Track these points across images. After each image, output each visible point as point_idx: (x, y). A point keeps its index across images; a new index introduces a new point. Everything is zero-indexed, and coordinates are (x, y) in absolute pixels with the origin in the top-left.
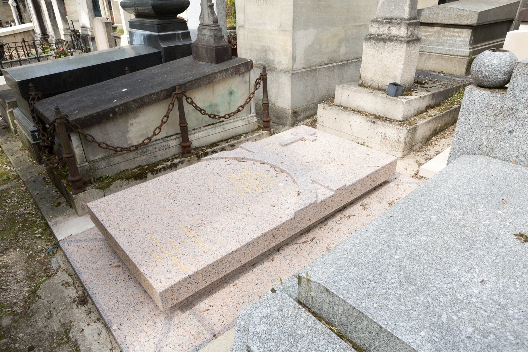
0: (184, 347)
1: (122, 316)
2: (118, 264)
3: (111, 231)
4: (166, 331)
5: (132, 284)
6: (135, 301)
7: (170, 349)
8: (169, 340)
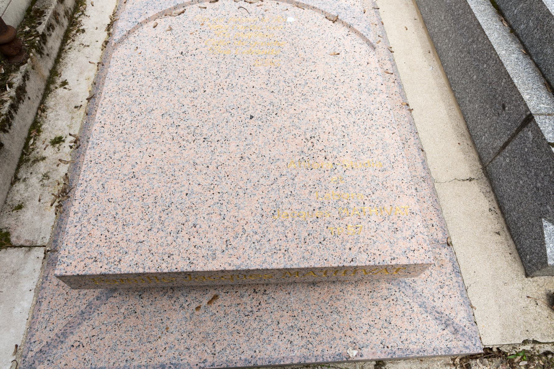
0: (447, 283)
1: (337, 335)
2: (209, 296)
3: (95, 269)
4: (411, 291)
5: (384, 287)
6: (323, 305)
7: (440, 300)
8: (426, 293)
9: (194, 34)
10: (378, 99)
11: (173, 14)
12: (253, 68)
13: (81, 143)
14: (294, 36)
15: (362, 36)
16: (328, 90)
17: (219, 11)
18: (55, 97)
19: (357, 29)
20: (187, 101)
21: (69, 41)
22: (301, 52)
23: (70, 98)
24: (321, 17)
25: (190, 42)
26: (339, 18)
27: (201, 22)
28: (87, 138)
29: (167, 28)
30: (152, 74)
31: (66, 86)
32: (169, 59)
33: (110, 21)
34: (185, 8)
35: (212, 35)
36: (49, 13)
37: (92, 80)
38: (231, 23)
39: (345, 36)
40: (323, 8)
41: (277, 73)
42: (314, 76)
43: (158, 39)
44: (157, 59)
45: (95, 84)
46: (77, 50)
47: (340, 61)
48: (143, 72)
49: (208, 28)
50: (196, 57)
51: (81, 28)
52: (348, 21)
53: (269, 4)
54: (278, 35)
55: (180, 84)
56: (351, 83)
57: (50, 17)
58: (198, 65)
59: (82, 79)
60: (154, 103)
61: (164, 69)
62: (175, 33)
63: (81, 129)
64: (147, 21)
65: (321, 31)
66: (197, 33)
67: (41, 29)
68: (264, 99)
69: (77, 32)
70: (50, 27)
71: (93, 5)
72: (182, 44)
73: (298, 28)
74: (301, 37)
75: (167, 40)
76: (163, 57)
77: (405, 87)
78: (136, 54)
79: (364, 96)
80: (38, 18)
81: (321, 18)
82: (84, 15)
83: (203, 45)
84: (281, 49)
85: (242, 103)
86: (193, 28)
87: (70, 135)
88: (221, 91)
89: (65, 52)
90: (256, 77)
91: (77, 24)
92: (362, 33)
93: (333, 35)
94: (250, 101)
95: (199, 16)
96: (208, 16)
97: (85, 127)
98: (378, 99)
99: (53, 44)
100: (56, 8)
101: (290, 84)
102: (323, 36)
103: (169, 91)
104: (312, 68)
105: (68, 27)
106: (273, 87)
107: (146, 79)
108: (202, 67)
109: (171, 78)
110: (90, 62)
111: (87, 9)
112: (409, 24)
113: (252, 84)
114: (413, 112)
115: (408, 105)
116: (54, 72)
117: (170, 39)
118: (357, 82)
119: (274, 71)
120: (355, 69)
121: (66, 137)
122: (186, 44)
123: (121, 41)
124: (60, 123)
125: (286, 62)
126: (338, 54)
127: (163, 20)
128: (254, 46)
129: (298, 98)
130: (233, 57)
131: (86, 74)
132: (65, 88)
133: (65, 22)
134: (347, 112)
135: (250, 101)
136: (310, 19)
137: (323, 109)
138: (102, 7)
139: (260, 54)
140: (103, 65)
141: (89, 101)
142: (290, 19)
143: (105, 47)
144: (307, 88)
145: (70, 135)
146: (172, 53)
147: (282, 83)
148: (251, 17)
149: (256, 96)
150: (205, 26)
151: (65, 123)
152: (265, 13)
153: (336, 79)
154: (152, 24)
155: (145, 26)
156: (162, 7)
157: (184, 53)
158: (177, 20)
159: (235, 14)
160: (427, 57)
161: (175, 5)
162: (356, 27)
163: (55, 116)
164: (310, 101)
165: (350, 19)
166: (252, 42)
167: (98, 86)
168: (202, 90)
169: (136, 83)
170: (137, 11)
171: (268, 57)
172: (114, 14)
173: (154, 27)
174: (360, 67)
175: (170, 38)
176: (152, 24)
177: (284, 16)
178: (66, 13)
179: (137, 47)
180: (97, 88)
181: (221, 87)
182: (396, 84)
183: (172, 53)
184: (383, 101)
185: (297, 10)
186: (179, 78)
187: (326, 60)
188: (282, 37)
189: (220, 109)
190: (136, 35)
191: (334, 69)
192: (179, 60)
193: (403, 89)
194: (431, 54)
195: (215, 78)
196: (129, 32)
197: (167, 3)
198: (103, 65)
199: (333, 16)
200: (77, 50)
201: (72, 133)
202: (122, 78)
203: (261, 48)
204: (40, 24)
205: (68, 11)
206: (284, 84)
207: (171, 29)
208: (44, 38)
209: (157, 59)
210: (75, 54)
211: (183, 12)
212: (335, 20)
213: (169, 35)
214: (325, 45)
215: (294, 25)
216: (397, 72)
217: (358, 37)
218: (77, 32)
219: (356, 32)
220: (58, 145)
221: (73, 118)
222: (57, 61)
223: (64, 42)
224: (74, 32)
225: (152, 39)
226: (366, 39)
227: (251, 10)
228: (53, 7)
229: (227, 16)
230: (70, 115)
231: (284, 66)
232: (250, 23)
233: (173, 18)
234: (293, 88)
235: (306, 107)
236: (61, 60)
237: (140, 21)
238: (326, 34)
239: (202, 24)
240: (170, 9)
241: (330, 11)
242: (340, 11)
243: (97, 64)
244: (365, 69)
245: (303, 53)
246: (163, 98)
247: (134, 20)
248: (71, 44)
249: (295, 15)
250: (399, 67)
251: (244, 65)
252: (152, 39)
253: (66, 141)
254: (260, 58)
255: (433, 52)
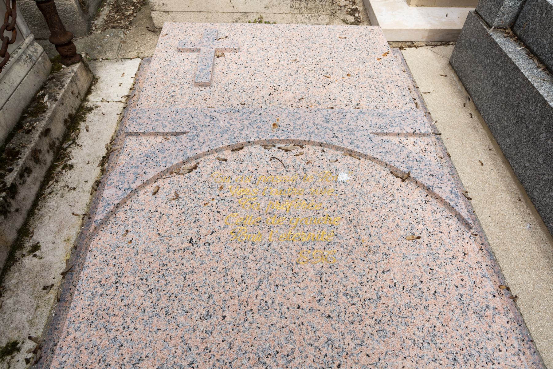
9: (210, 204)
10: (496, 328)
11: (182, 172)
12: (296, 268)
13: (43, 354)
14: (351, 206)
15: (447, 205)
16: (414, 312)
17: (244, 164)
18: (20, 270)
19: (440, 195)
20: (194, 340)
21: (51, 182)
22: (364, 236)
23: (39, 272)
24: (385, 172)
25: (204, 218)
26: (412, 175)
27: (220, 183)
28: (52, 344)
29: (173, 195)
30: (145, 281)
31: (37, 253)
32: (171, 253)
33: (106, 151)
34: (199, 161)
35: (235, 205)
36: (26, 153)
37: (72, 241)
38: (262, 185)
39: (423, 205)
40: (386, 159)
41: (333, 278)
42: (388, 283)
43: (158, 214)
44: (155, 253)
45: (76, 248)
46: (59, 195)
47: (423, 252)
48: (132, 279)
49: (229, 195)
50: (211, 248)
51: (68, 163)
52: (425, 180)
53: (311, 152)
54: (328, 205)
55: (187, 303)
56: (446, 294)
57: (27, 159)
58: (213, 264)
59: (59, 241)
60: (143, 345)
61: (164, 272)
62: (183, 203)
63: (46, 326)
64: (144, 185)
65: (388, 195)
66: (214, 203)
67: (10, 179)
68: (318, 333)
69: (63, 169)
70: (26, 171)
71: (87, 131)
72: (192, 224)
73: (355, 191)
74: (361, 207)
75: (171, 217)
76: (162, 247)
77: (497, 256)
78: (125, 244)
79: (472, 321)
80: (10, 162)
81: (385, 173)
82: (76, 143)
83: (222, 224)
84: (334, 230)
85: (283, 342)
86: (208, 195)
87: (30, 338)
88: (249, 316)
89: (44, 198)
90: (302, 285)
91: (65, 157)
92: (448, 201)
93: (405, 202)
94: (295, 337)
95: (216, 173)
96: (230, 173)
97: (53, 324)
98: (496, 328)
99: (28, 192)
100: (36, 144)
101: (356, 300)
102: (392, 205)
103: (169, 317)
104: (383, 265)
105: (53, 163)
106: (329, 306)
107: (135, 292)
108: (220, 266)
109: (172, 289)
110: (73, 214)
111: (80, 136)
112: (485, 157)
113: (296, 300)
114: (518, 302)
115: (508, 289)
116: (25, 231)
117: (175, 214)
118: (455, 293)
119: (328, 273)
120: (448, 266)
121: (23, 343)
122: (198, 223)
123: (105, 221)
124: (18, 315)
125: (345, 255)
126: (419, 238)
127: (167, 181)
128: (295, 227)
129: (369, 330)
130: (266, 246)
131: (66, 232)
132: (35, 256)
133: (49, 158)
134: (451, 357)
135: (295, 337)
136: (370, 175)
137: (412, 353)
138: (99, 132)
139: (305, 239)
140: (90, 218)
141: (64, 278)
142: (343, 177)
143: (96, 190)
144: (381, 308)
145: (30, 338)
146: (176, 242)
147: (342, 299)
148: (288, 174)
149: (305, 327)
150: (225, 190)
151: (25, 316)
152: (307, 166)
153: (424, 287)
154: (151, 188)
155: (141, 192)
156: (166, 162)
157: (194, 240)
158: (187, 180)
159: (265, 169)
160: (518, 207)
161: (184, 158)
162: (437, 191)
163: (15, 303)
164: (389, 335)
165: (427, 177)
166: (292, 219)
167: (80, 252)
168: (220, 313)
169: (119, 302)
170: (132, 171)
171: (317, 246)
172: (113, 141)
173: (154, 194)
174: (454, 261)
175: (175, 212)
176: (151, 188)
177: (333, 170)
178: (51, 146)
179: (127, 231)
180: (78, 256)
181: (248, 308)
182: (485, 251)
183: (176, 242)
184: (503, 331)
185: (352, 161)
186: (185, 289)
187: (403, 251)
188: (333, 207)
189: (247, 355)
190: (127, 208)
191: (416, 267)
192: (187, 254)
193: (495, 261)
194: (523, 203)
195: (239, 288)
196: (117, 206)
197: (174, 157)
198: (90, 218)
199: (402, 172)
200: (59, 195)
201: (33, 335)
202: (100, 290)
203: (306, 229)
204: (11, 171)
205: (54, 143)
206: (344, 298)
207: (177, 197)
208: (13, 191)
209: (155, 253)
210: (56, 202)
211: (195, 167)
212: (405, 177)
213: (175, 208)
214: (397, 221)
215: (349, 187)
216: (482, 231)
217: (441, 207)
218: (63, 169)
219: (438, 198)
220: (9, 357)
221: (38, 307)
222: (31, 213)
223: (44, 184)
224: (59, 169)
225: (150, 215)
226: (455, 211)
227: (288, 162)
228: (33, 145)
229: (255, 172)
230: (35, 302)
231: (342, 263)
232: (287, 184)
233: (181, 178)
234: (361, 309)
235: (385, 350)
236: (36, 211)
237: (134, 186)
238: (395, 202)
239: (221, 188)
240: (178, 164)
241: (397, 165)
242: (410, 164)
243: (82, 216)
244: (462, 264)
245: (367, 237)
246: (160, 333)
247: (126, 186)
248: (53, 186)
249: (350, 170)
250: (483, 223)
251: (282, 261)
252: (150, 215)
253: (22, 350)
254: (305, 248)
255: (525, 199)
